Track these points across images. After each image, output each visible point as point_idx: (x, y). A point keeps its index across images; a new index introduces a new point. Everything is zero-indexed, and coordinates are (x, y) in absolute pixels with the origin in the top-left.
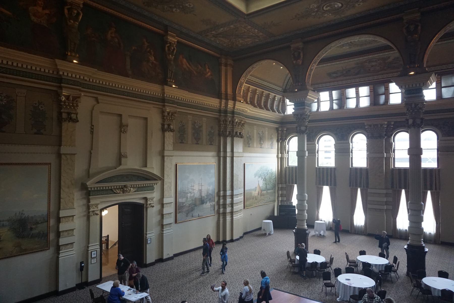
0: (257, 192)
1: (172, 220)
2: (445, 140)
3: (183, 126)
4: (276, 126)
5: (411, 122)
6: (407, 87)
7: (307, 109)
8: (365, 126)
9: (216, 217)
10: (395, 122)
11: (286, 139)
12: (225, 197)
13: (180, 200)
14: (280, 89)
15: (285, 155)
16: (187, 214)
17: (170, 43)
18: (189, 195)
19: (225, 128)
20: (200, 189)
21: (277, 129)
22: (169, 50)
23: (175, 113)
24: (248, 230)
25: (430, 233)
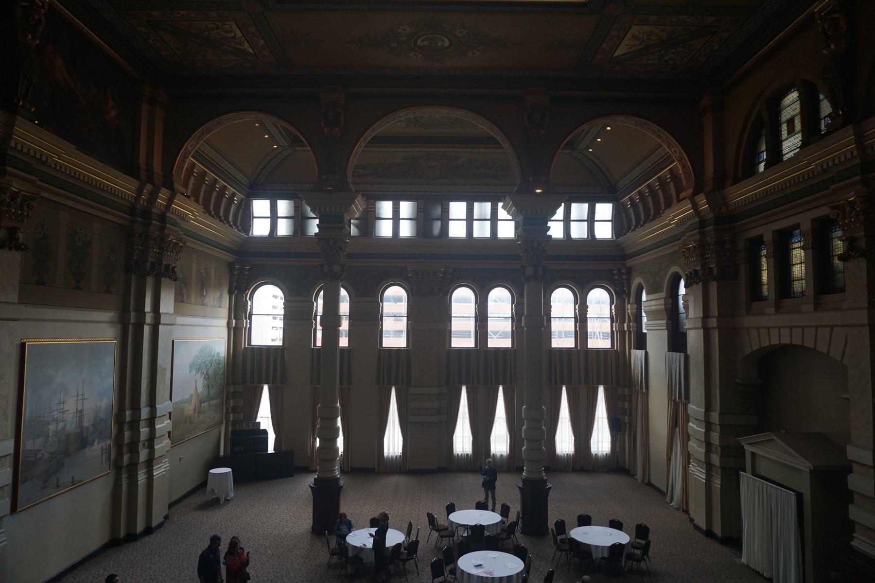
0: (192, 407)
4: (229, 258)
5: (530, 271)
9: (111, 478)
12: (135, 424)
13: (27, 445)
14: (245, 181)
18: (52, 427)
20: (79, 408)
21: (231, 266)
24: (175, 498)
25: (501, 455)
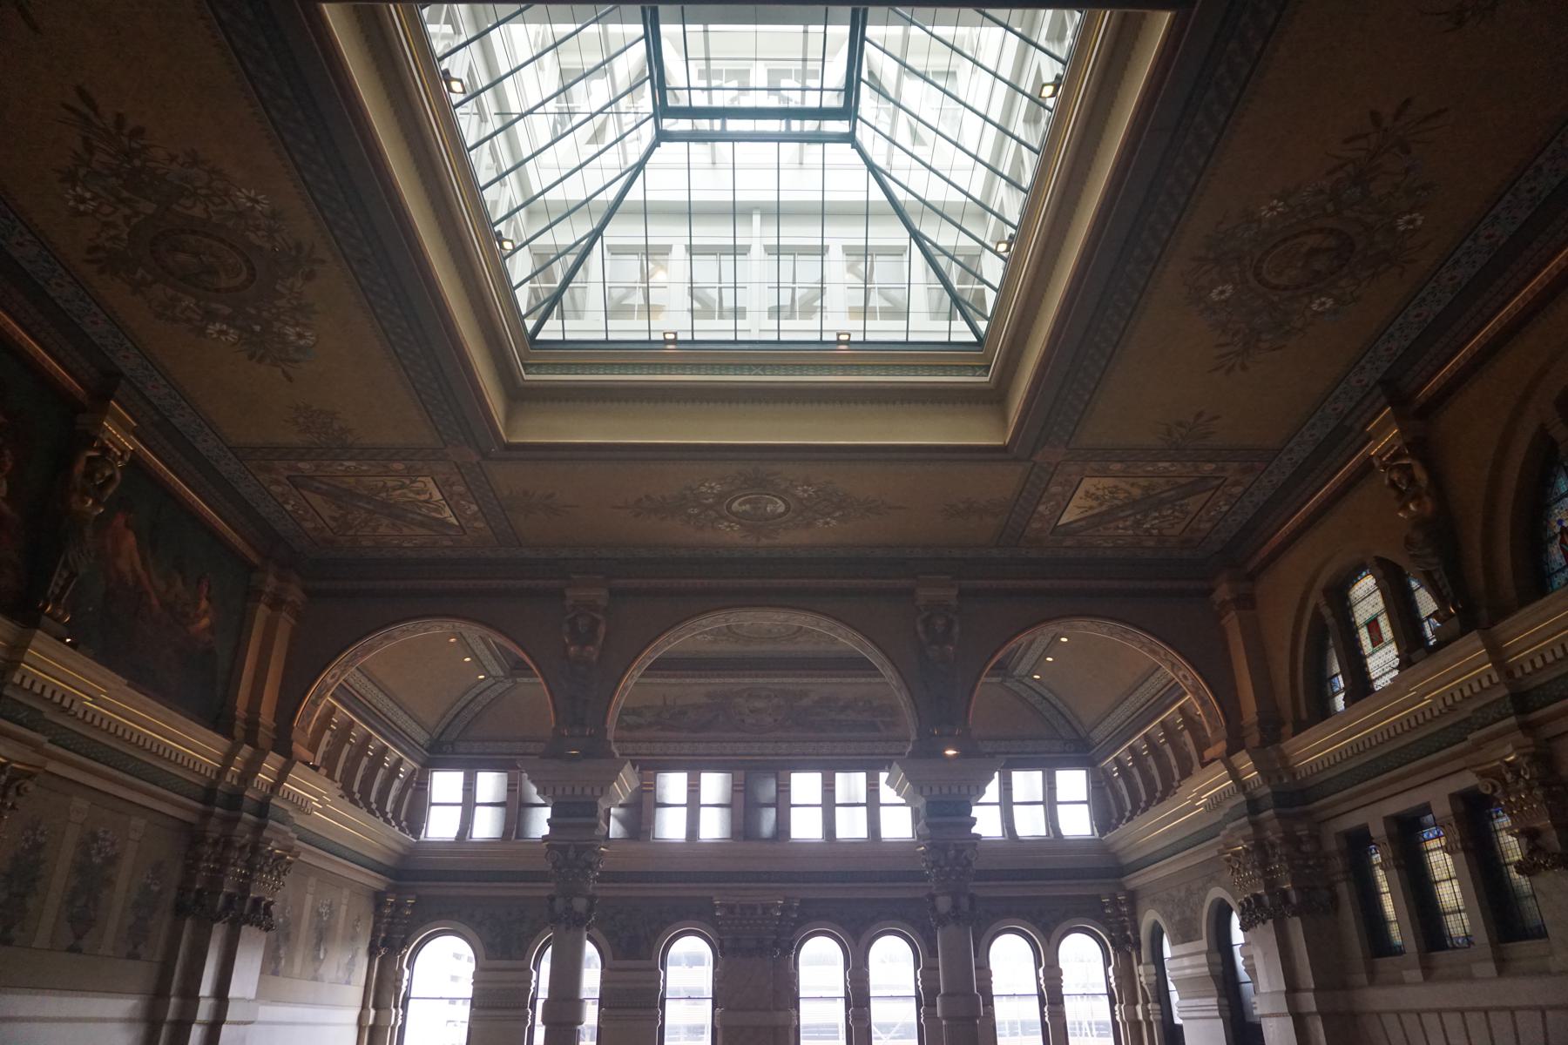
2: (497, 970)
3: (38, 847)
4: (376, 882)
6: (559, 792)
7: (277, 831)
8: (714, 908)
10: (802, 901)
11: (405, 944)
17: (105, 450)
19: (215, 881)
21: (378, 899)
22: (89, 475)
23: (30, 776)
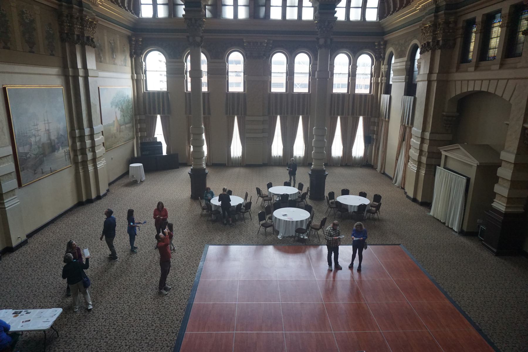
0: (115, 128)
1: (14, 183)
4: (128, 32)
5: (322, 41)
12: (82, 138)
13: (20, 150)
15: (143, 76)
16: (35, 170)
20: (47, 128)
21: (129, 38)
